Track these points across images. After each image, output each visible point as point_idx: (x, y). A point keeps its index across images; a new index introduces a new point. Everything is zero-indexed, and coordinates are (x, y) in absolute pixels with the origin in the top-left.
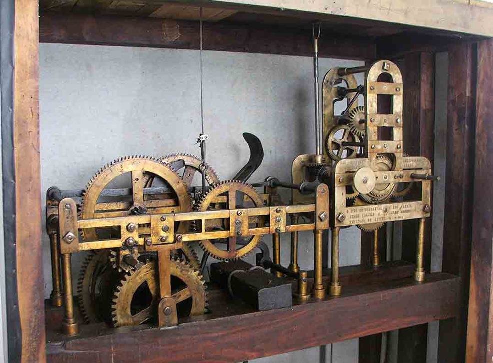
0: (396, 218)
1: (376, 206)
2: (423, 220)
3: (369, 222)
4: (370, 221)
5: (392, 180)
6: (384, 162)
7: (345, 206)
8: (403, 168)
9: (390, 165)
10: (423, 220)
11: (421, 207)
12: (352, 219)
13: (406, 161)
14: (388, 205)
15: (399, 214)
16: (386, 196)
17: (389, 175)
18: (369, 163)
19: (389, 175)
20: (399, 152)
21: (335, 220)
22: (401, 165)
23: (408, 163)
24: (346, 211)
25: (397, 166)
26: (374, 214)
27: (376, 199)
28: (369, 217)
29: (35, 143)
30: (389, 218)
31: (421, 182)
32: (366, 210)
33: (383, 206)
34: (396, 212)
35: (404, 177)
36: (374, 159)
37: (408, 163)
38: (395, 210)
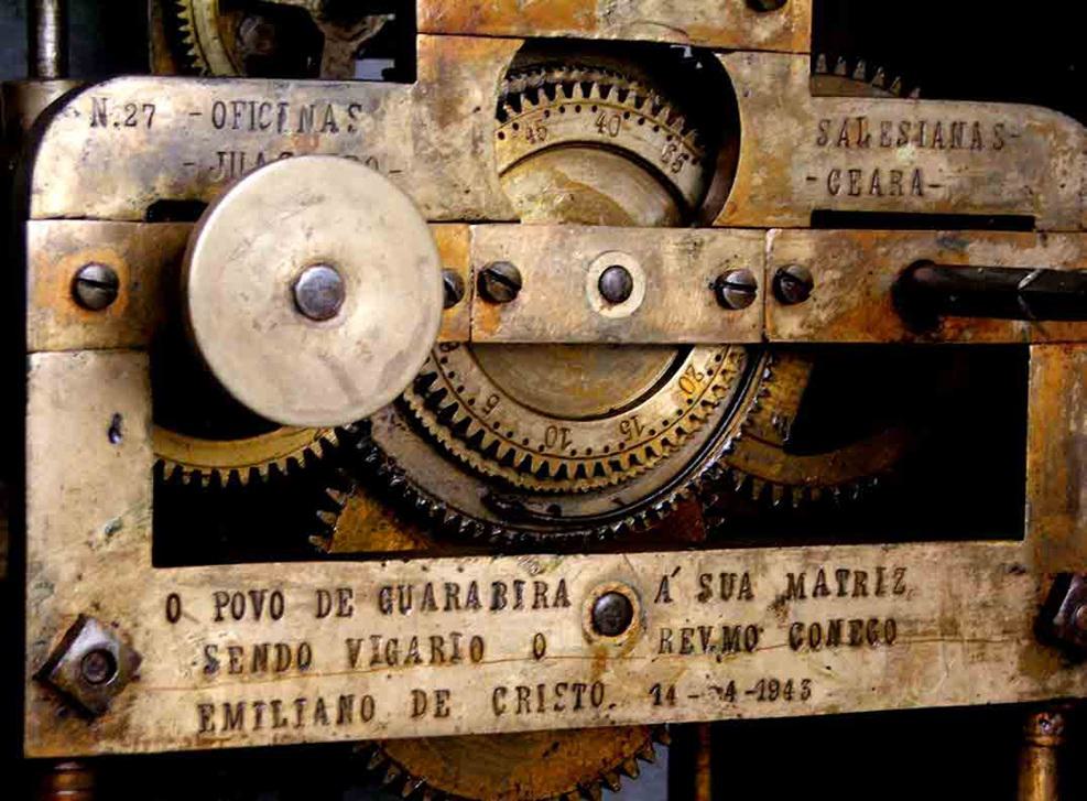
0: (731, 691)
1: (506, 567)
2: (1045, 732)
3: (429, 726)
4: (806, 695)
5: (689, 311)
6: (623, 140)
7: (146, 549)
8: (818, 198)
9: (685, 179)
10: (1045, 732)
11: (1018, 595)
12: (221, 691)
13: (855, 137)
14: (645, 565)
15: (773, 660)
16: (686, 454)
17: (653, 267)
18: (433, 134)
19: (653, 267)
20: (778, 46)
21: (32, 693)
22: (798, 178)
23: (869, 162)
24: (154, 600)
25: (748, 176)
26: (478, 645)
27: (539, 508)
28: (427, 677)
29: (578, 188)
30: (661, 694)
31: (1014, 359)
32: (385, 600)
33: (583, 573)
34: (739, 641)
35: (820, 295)
36: (481, 91)
37: (869, 162)
38: (715, 616)
